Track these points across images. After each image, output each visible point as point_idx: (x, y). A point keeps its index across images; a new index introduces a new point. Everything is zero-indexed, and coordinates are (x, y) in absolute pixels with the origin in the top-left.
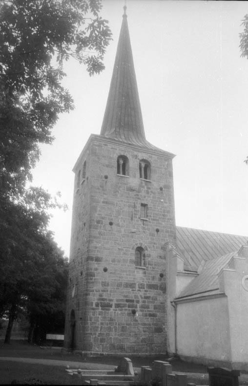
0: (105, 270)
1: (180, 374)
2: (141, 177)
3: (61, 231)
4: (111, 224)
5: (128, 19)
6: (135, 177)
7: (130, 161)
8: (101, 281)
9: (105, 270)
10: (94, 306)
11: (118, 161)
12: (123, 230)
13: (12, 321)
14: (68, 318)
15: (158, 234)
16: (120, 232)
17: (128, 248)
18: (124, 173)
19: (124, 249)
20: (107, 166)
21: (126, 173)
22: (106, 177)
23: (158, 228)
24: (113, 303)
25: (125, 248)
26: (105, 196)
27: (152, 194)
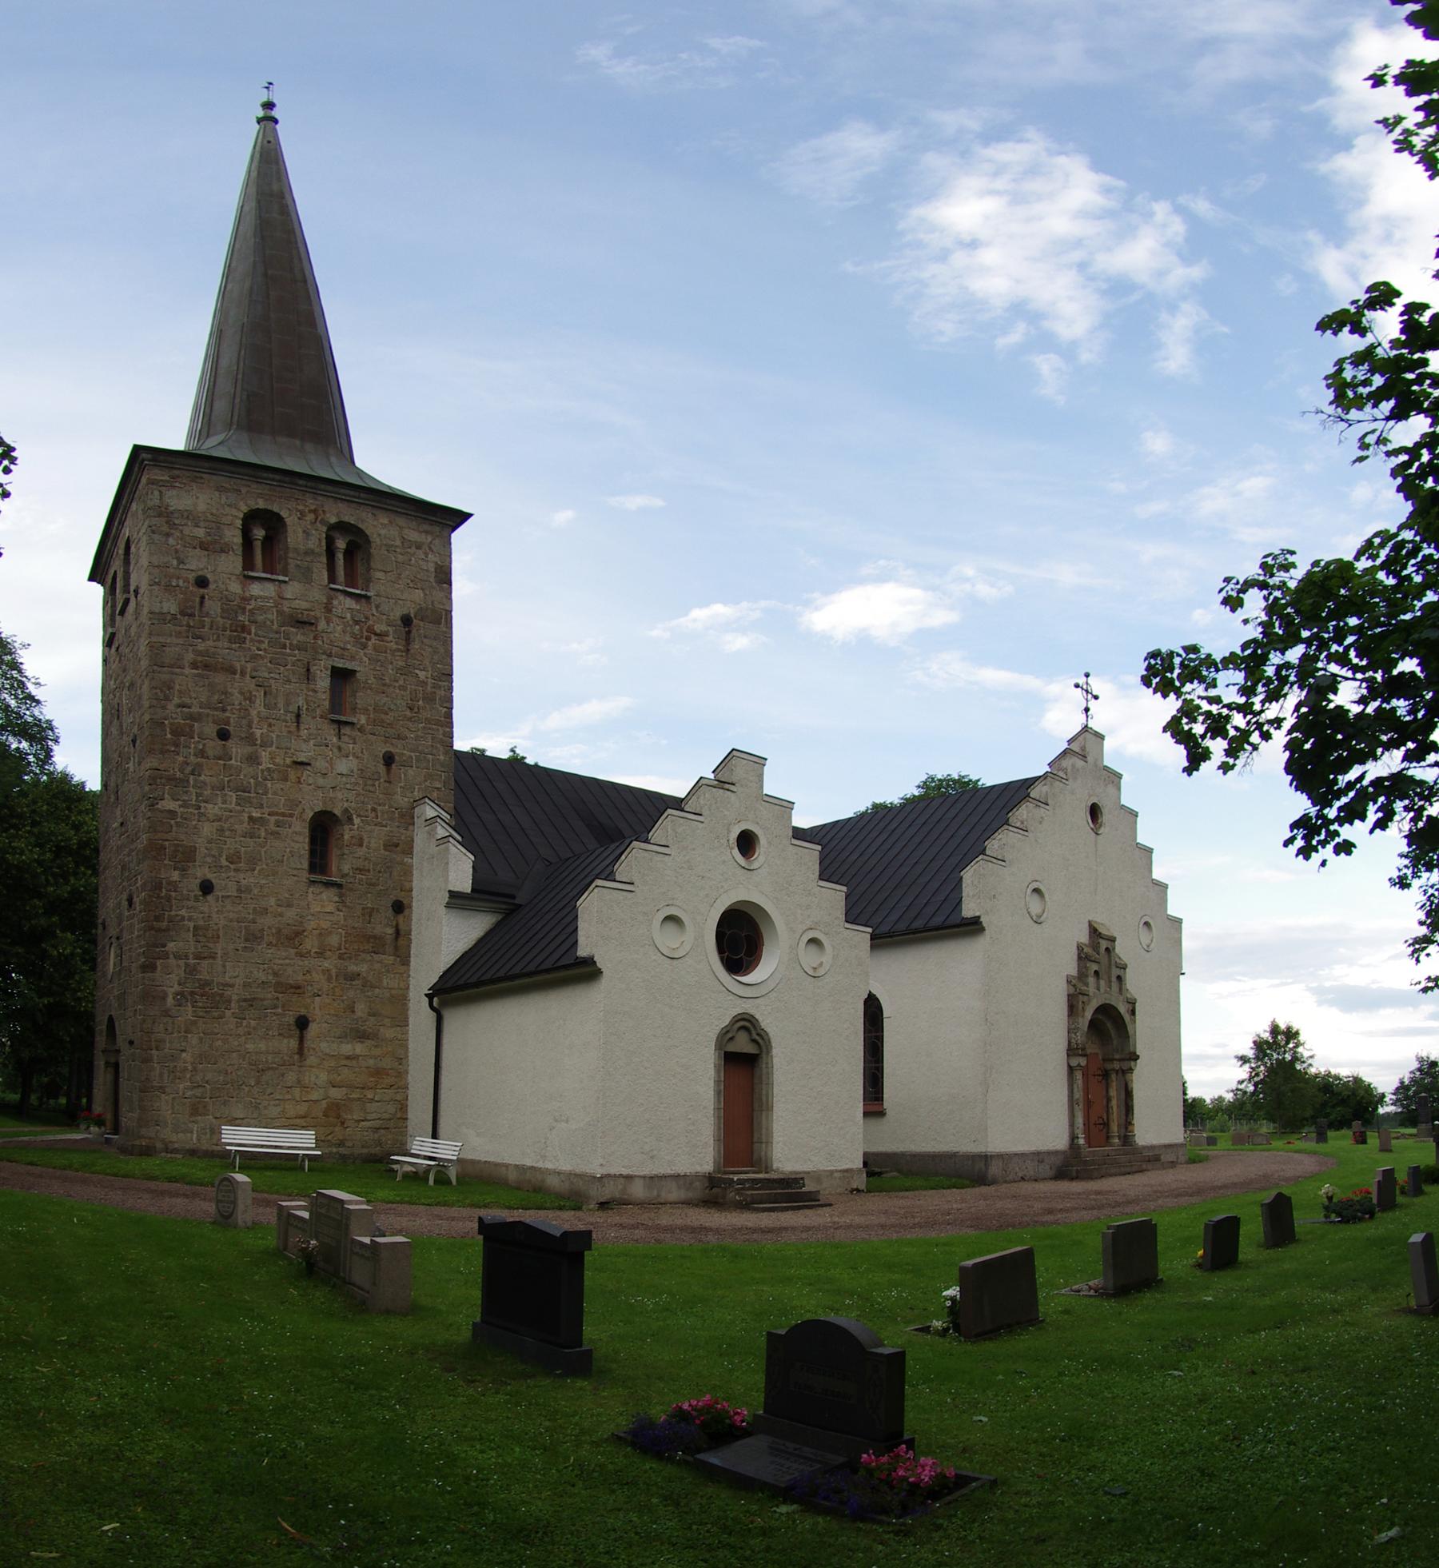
2: (332, 579)
3: (80, 758)
4: (223, 735)
5: (285, 133)
6: (307, 576)
7: (290, 530)
8: (191, 924)
9: (207, 888)
11: (330, 542)
12: (264, 755)
14: (101, 1027)
15: (388, 771)
16: (253, 759)
17: (283, 814)
18: (269, 568)
19: (273, 819)
20: (204, 546)
21: (279, 567)
23: (210, 876)
24: (234, 994)
25: (277, 814)
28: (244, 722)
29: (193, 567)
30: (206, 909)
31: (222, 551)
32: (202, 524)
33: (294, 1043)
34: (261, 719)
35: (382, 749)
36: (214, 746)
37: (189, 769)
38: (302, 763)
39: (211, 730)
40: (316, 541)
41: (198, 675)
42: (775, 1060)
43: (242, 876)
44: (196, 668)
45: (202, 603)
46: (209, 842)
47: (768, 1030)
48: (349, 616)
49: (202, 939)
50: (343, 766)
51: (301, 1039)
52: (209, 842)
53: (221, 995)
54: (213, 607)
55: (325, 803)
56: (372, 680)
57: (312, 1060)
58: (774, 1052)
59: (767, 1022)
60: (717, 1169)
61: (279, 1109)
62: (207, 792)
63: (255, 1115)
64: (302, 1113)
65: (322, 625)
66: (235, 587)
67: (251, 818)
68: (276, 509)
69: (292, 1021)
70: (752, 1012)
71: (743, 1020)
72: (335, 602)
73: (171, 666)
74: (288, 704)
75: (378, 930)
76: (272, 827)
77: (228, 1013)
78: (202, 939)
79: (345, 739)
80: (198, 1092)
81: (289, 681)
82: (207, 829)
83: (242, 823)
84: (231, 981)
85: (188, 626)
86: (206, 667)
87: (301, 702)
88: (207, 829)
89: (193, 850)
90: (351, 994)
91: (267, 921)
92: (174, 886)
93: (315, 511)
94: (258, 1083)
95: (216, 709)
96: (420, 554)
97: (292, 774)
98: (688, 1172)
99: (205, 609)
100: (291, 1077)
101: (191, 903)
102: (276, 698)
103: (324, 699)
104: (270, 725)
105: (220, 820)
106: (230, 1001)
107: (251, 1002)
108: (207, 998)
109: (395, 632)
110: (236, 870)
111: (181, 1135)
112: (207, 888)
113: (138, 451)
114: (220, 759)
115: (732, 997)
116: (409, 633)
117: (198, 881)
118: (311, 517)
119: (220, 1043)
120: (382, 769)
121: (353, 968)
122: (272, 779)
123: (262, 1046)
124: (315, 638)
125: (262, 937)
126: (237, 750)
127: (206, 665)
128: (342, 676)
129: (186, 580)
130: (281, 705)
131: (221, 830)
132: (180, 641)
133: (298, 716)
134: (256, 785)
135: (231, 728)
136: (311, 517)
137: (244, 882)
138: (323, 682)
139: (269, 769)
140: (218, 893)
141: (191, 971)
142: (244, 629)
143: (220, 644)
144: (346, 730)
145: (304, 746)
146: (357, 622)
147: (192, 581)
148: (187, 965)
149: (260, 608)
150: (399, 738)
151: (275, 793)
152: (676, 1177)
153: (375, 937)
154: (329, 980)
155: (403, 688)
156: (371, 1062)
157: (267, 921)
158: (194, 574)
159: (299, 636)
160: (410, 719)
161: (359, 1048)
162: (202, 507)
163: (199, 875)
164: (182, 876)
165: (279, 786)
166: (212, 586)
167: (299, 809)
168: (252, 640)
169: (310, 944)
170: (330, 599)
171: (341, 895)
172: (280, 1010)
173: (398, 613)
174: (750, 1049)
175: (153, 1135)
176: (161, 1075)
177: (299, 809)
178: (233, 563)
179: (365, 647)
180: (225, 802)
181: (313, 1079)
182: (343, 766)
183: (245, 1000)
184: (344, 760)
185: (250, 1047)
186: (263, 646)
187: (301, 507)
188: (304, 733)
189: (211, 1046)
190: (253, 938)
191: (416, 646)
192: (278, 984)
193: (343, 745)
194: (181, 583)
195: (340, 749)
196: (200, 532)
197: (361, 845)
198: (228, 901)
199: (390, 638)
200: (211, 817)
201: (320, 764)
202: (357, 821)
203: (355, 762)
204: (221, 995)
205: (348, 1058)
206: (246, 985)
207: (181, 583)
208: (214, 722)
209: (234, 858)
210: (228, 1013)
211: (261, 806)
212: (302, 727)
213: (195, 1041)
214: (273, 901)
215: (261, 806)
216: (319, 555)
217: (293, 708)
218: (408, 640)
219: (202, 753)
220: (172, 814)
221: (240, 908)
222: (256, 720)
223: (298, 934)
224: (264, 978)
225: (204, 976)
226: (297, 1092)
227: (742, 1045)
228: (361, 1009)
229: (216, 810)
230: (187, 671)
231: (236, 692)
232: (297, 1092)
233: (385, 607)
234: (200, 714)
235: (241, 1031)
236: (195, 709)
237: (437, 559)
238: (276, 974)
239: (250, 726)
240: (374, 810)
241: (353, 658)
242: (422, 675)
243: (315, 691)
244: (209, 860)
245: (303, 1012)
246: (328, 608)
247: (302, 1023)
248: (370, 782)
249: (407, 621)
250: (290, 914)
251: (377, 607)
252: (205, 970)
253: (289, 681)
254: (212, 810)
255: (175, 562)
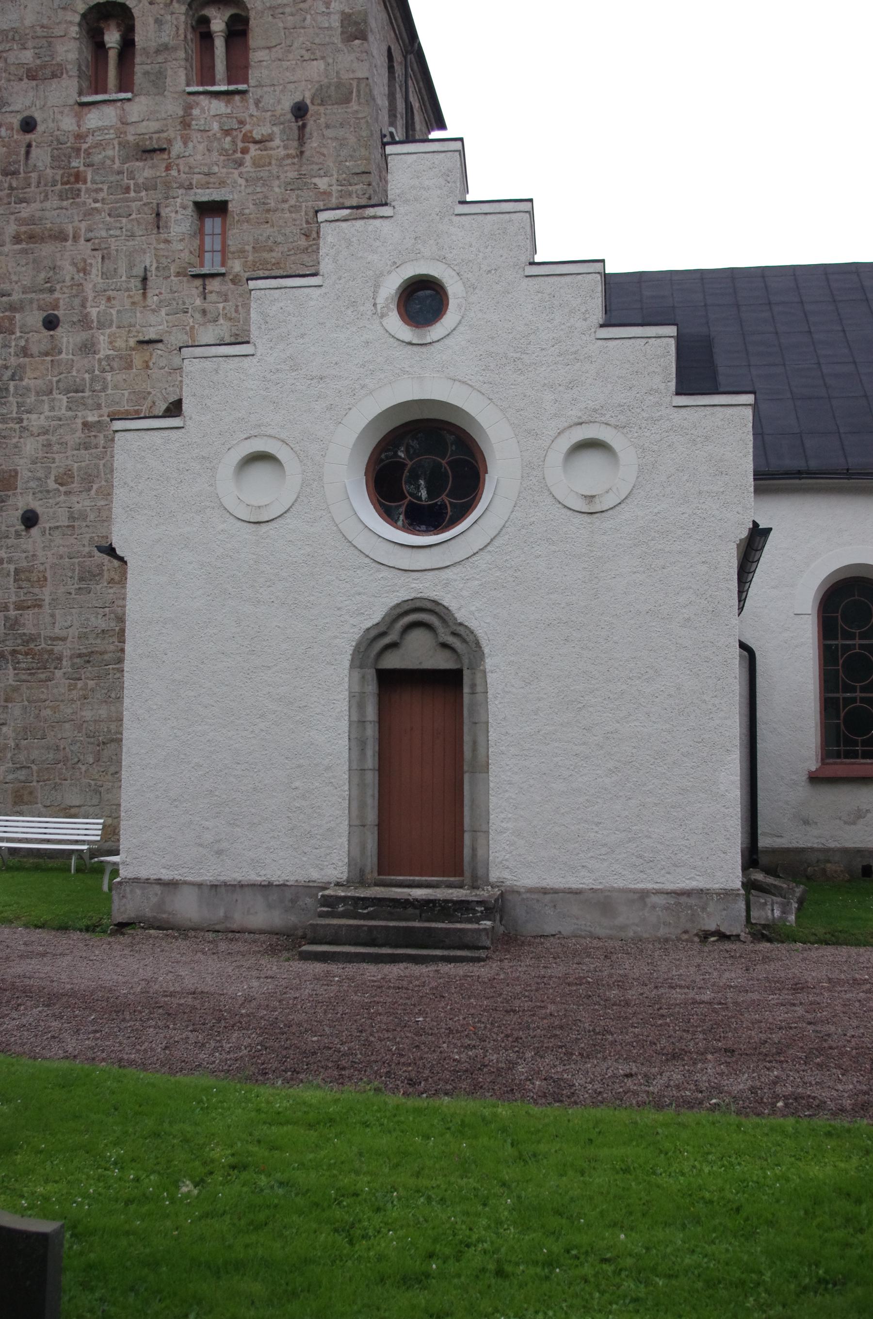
8: (12, 567)
12: (102, 340)
16: (88, 348)
20: (32, 75)
24: (64, 649)
28: (77, 302)
29: (16, 108)
30: (30, 547)
31: (54, 76)
32: (30, 44)
34: (98, 293)
36: (40, 339)
39: (35, 318)
41: (24, 252)
42: (491, 678)
43: (75, 499)
45: (28, 153)
46: (34, 463)
47: (472, 624)
49: (24, 584)
52: (34, 463)
53: (51, 652)
54: (41, 156)
56: (250, 209)
58: (489, 663)
59: (467, 609)
60: (359, 879)
62: (31, 399)
65: (177, 148)
66: (68, 123)
67: (85, 424)
70: (433, 594)
71: (407, 613)
74: (131, 266)
77: (58, 673)
78: (24, 584)
79: (212, 297)
80: (22, 775)
82: (30, 447)
83: (73, 431)
84: (63, 633)
85: (11, 188)
86: (31, 238)
87: (148, 260)
88: (30, 447)
89: (14, 474)
97: (138, 359)
98: (292, 879)
99: (31, 162)
101: (10, 542)
104: (109, 299)
105: (46, 433)
106: (60, 659)
109: (283, 132)
110: (67, 493)
112: (30, 520)
114: (47, 354)
115: (385, 573)
117: (20, 513)
119: (49, 712)
122: (112, 369)
124: (168, 168)
125: (101, 574)
126: (67, 337)
130: (122, 270)
133: (145, 279)
134: (92, 380)
135: (59, 313)
137: (77, 507)
140: (45, 523)
142: (78, 177)
143: (48, 205)
144: (214, 285)
145: (152, 319)
146: (227, 132)
149: (98, 145)
151: (116, 387)
152: (266, 887)
155: (295, 209)
158: (20, 117)
159: (145, 171)
165: (121, 377)
166: (40, 128)
170: (188, 108)
173: (287, 104)
174: (442, 662)
178: (66, 89)
179: (240, 164)
180: (52, 409)
183: (80, 656)
184: (210, 327)
185: (88, 714)
186: (100, 196)
189: (37, 716)
191: (313, 144)
195: (204, 312)
196: (27, 56)
198: (57, 533)
199: (277, 142)
200: (35, 431)
204: (51, 652)
206: (83, 636)
208: (40, 308)
210: (58, 673)
211: (99, 407)
212: (150, 294)
215: (99, 407)
216: (175, 49)
217: (139, 271)
218: (301, 138)
219: (25, 352)
221: (72, 540)
222: (90, 295)
225: (29, 629)
227: (419, 653)
229: (42, 421)
233: (268, 101)
234: (21, 301)
235: (75, 694)
236: (15, 297)
239: (83, 306)
241: (222, 183)
244: (32, 484)
246: (185, 123)
251: (257, 103)
252: (29, 623)
253: (133, 235)
254: (35, 421)
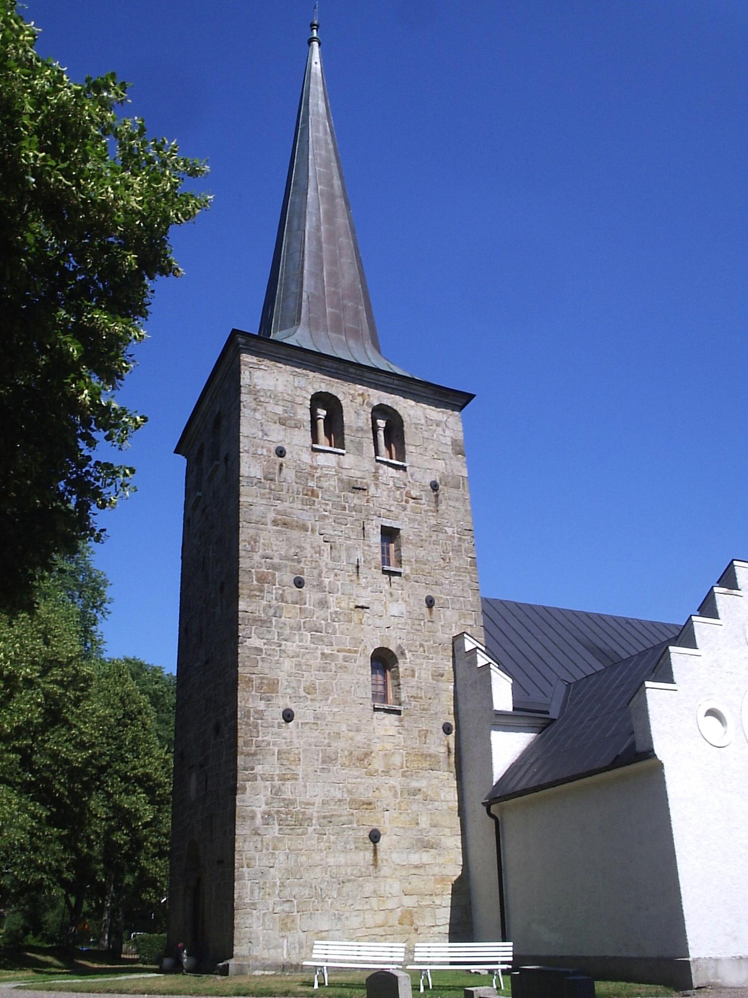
0: (288, 716)
1: (322, 105)
4: (299, 583)
6: (359, 449)
9: (288, 716)
10: (258, 821)
12: (331, 599)
13: (57, 684)
16: (323, 604)
17: (349, 651)
19: (341, 655)
20: (282, 422)
22: (281, 453)
26: (280, 506)
27: (411, 501)
28: (316, 572)
33: (369, 855)
35: (424, 593)
37: (272, 611)
38: (363, 607)
39: (289, 578)
40: (364, 419)
41: (278, 532)
43: (318, 705)
44: (277, 525)
48: (391, 484)
50: (395, 609)
51: (375, 851)
53: (304, 813)
54: (289, 474)
55: (382, 641)
57: (385, 871)
61: (360, 919)
62: (287, 631)
63: (339, 927)
64: (379, 922)
65: (372, 490)
66: (306, 457)
67: (323, 654)
68: (333, 391)
69: (367, 835)
72: (381, 471)
73: (257, 523)
74: (349, 557)
75: (433, 750)
76: (340, 661)
77: (310, 829)
80: (286, 907)
81: (349, 538)
82: (288, 664)
83: (316, 658)
84: (312, 800)
85: (271, 489)
87: (359, 555)
88: (288, 664)
90: (415, 807)
91: (339, 745)
92: (260, 714)
93: (362, 395)
94: (339, 894)
95: (293, 560)
96: (439, 429)
97: (356, 616)
100: (369, 887)
101: (276, 730)
102: (339, 551)
103: (377, 551)
104: (336, 575)
105: (298, 656)
107: (329, 819)
108: (293, 819)
111: (272, 951)
113: (233, 330)
116: (437, 496)
117: (281, 710)
118: (359, 400)
120: (426, 610)
121: (415, 784)
123: (342, 859)
126: (310, 594)
127: (284, 523)
128: (390, 534)
129: (269, 451)
131: (298, 665)
132: (264, 502)
135: (305, 577)
136: (359, 400)
137: (319, 711)
138: (376, 538)
139: (336, 612)
141: (276, 792)
143: (295, 505)
144: (395, 579)
145: (363, 593)
146: (398, 488)
147: (273, 450)
148: (273, 787)
150: (436, 584)
153: (430, 755)
154: (395, 795)
156: (436, 870)
157: (339, 745)
159: (355, 499)
160: (443, 569)
161: (426, 857)
162: (280, 388)
163: (281, 704)
164: (268, 706)
165: (345, 626)
167: (362, 647)
168: (319, 503)
169: (377, 764)
170: (377, 469)
171: (401, 721)
172: (355, 825)
173: (428, 481)
175: (246, 953)
176: (252, 892)
177: (362, 647)
179: (405, 509)
181: (387, 888)
182: (395, 609)
183: (324, 817)
184: (395, 604)
185: (331, 861)
187: (352, 392)
188: (363, 581)
190: (329, 759)
191: (442, 507)
192: (352, 801)
193: (394, 591)
194: (265, 453)
195: (391, 594)
196: (279, 410)
197: (413, 676)
198: (307, 727)
199: (423, 501)
201: (376, 607)
202: (408, 655)
203: (404, 605)
204: (304, 813)
205: (416, 867)
207: (265, 453)
209: (310, 690)
213: (282, 858)
214: (344, 728)
219: (282, 598)
220: (259, 650)
222: (325, 570)
223: (367, 755)
224: (339, 796)
225: (288, 795)
226: (374, 901)
228: (424, 822)
230: (270, 527)
231: (308, 546)
232: (374, 901)
235: (322, 845)
236: (276, 560)
237: (452, 435)
238: (349, 792)
239: (320, 575)
240: (422, 645)
241: (396, 518)
242: (449, 531)
243: (369, 546)
245: (375, 825)
247: (375, 837)
248: (417, 622)
249: (435, 486)
250: (360, 738)
251: (412, 475)
255: (260, 434)
